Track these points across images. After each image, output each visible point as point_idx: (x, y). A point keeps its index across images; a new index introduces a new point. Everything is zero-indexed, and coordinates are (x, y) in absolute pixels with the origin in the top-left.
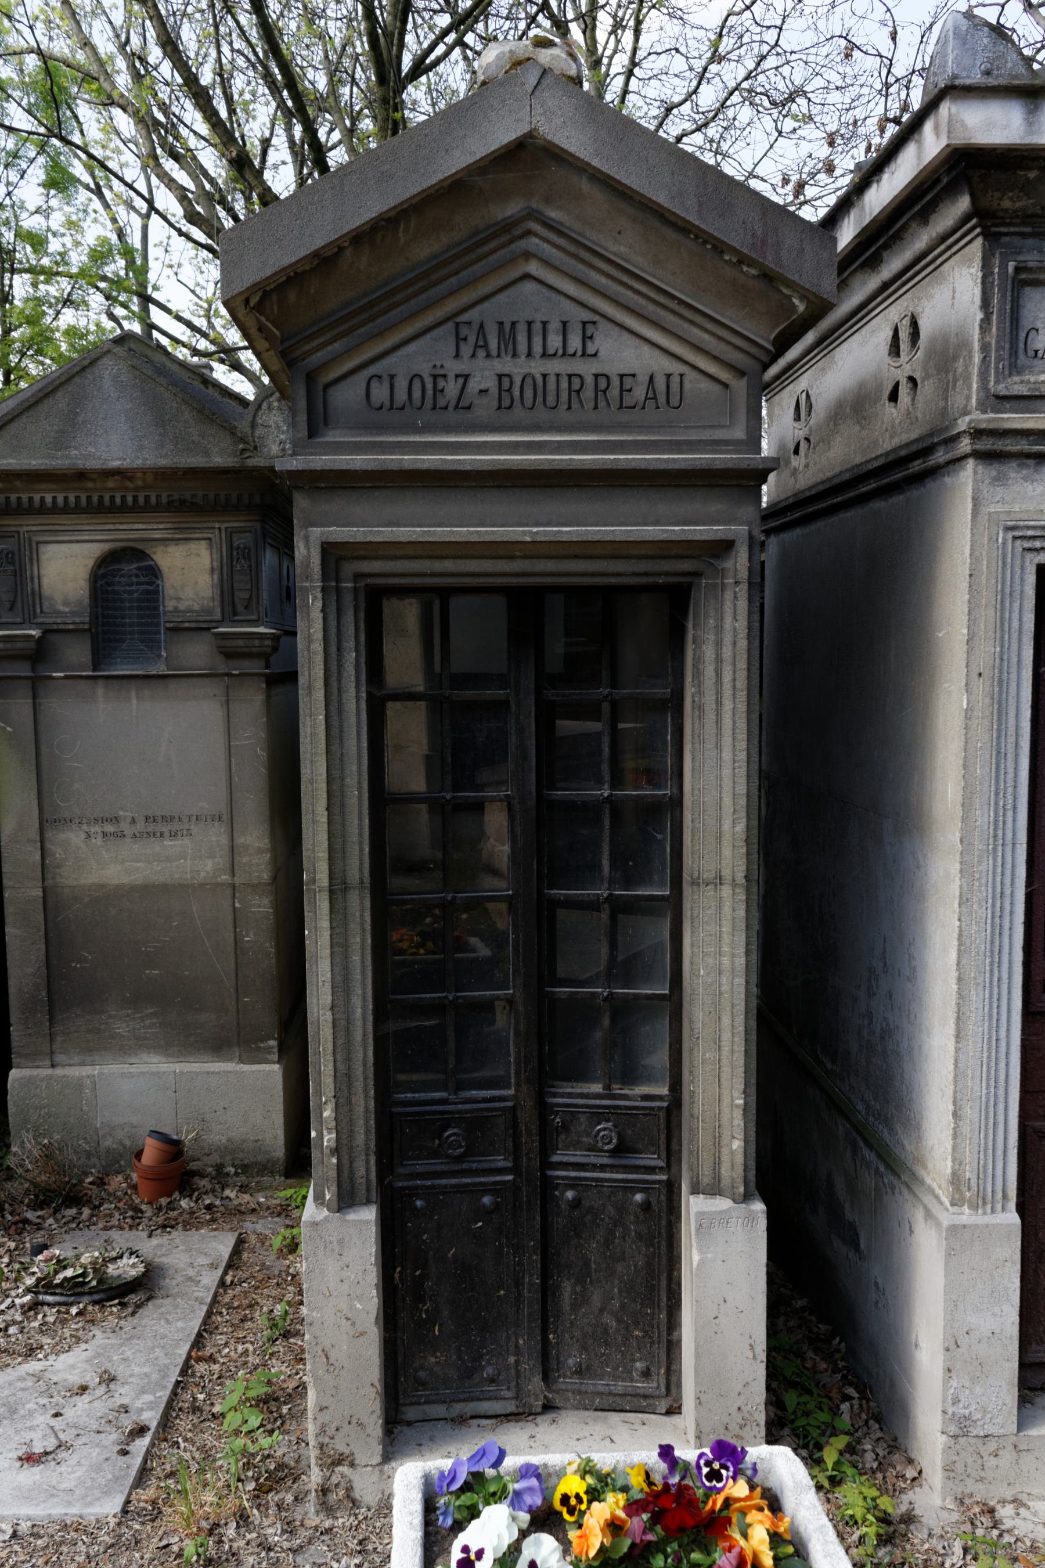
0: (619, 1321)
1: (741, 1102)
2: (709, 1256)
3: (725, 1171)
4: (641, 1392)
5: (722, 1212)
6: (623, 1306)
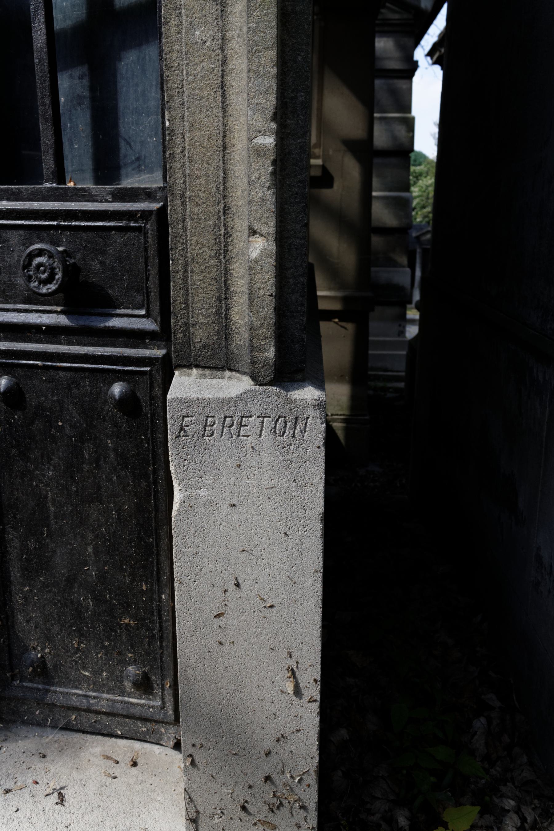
0: (98, 600)
1: (269, 141)
2: (203, 493)
3: (241, 316)
4: (136, 711)
5: (226, 402)
6: (102, 577)
